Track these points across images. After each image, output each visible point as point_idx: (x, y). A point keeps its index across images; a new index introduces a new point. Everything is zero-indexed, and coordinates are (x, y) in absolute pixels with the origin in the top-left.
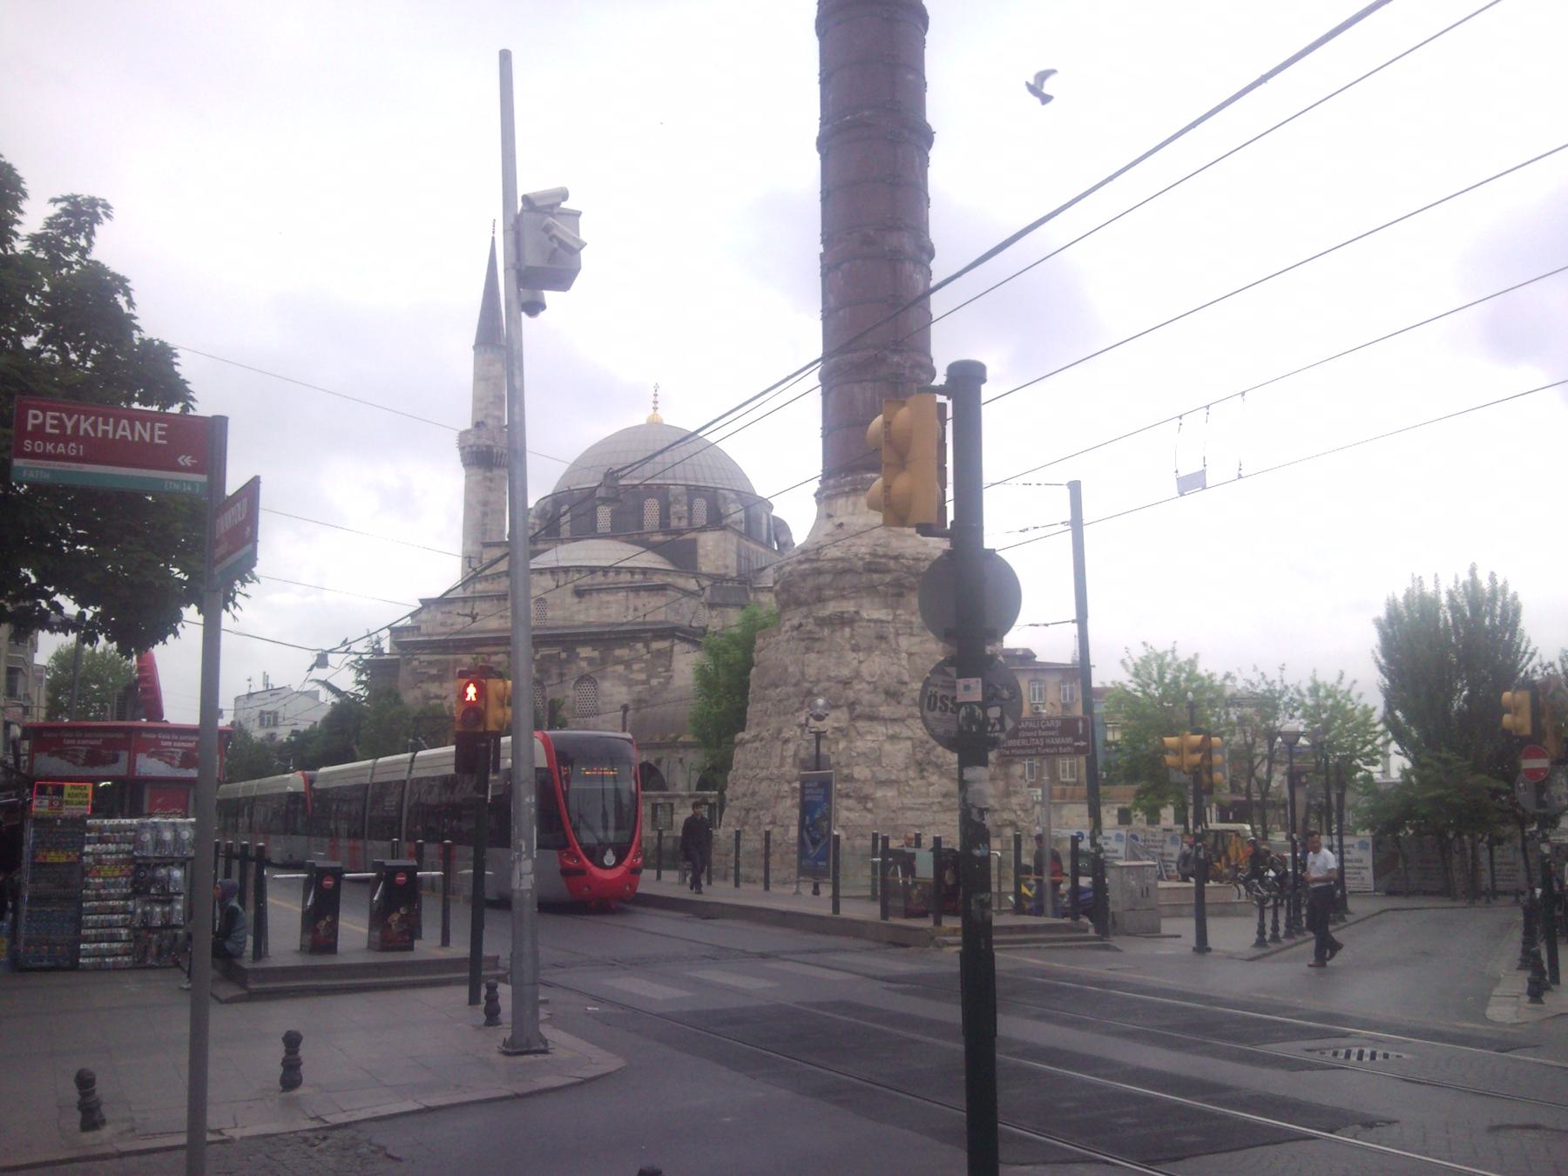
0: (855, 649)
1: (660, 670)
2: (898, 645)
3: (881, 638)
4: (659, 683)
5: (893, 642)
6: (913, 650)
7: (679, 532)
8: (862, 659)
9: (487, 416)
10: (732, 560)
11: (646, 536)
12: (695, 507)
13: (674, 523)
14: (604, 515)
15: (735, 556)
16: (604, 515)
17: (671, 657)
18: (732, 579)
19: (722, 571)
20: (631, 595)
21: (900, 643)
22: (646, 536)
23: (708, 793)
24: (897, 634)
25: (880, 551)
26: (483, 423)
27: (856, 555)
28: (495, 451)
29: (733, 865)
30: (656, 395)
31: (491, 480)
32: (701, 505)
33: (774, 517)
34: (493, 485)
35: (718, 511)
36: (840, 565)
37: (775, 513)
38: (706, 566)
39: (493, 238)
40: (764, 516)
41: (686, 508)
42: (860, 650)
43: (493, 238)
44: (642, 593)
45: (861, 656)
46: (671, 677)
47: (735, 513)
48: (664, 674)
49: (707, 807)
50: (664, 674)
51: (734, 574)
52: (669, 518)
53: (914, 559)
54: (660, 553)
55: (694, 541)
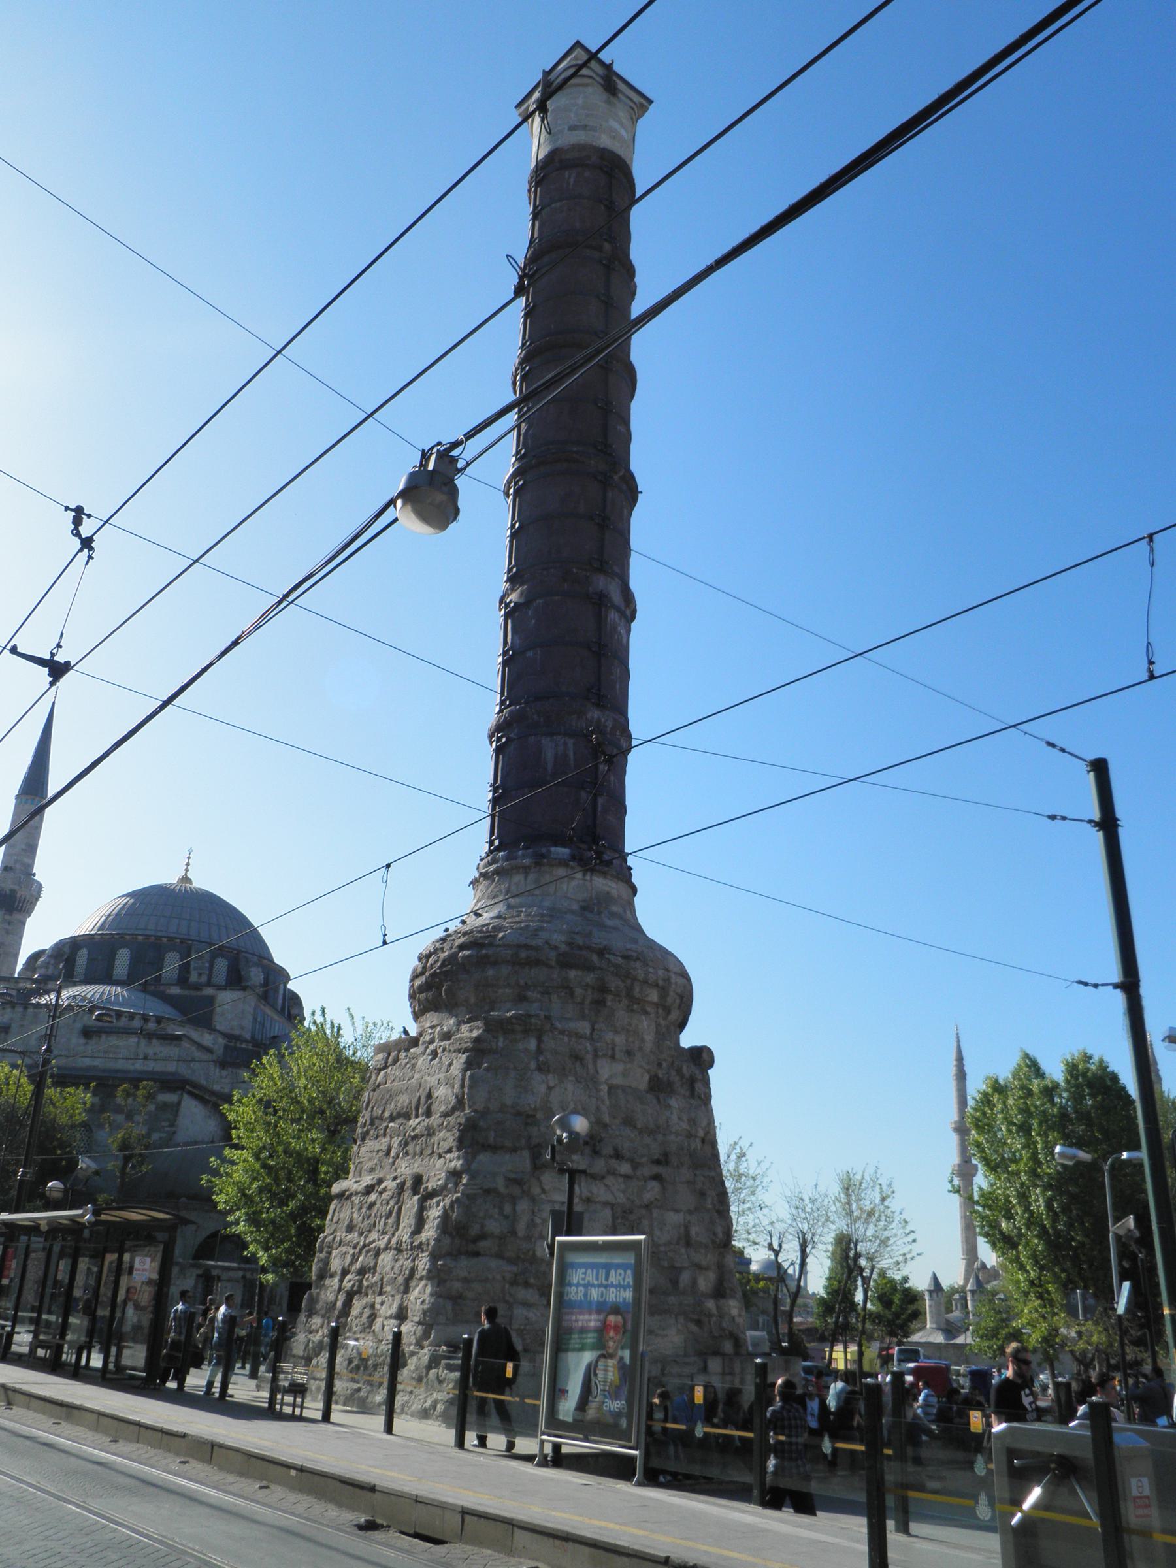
0: (542, 1069)
1: (164, 1124)
2: (597, 1072)
3: (577, 1058)
4: (161, 1138)
5: (590, 1066)
6: (618, 1081)
7: (197, 987)
8: (551, 1084)
9: (16, 861)
10: (247, 1023)
11: (162, 988)
12: (216, 967)
13: (193, 978)
14: (123, 958)
15: (250, 1018)
16: (123, 958)
17: (177, 1111)
18: (246, 1041)
19: (237, 1032)
20: (143, 1042)
21: (601, 1071)
22: (162, 988)
23: (212, 1263)
24: (596, 1056)
25: (580, 941)
26: (11, 868)
27: (547, 943)
28: (18, 895)
29: (324, 1375)
30: (189, 858)
31: (9, 923)
32: (222, 965)
33: (290, 990)
34: (10, 928)
35: (239, 971)
36: (523, 954)
37: (291, 986)
38: (221, 1024)
39: (54, 703)
40: (282, 986)
41: (207, 965)
42: (549, 1071)
43: (54, 703)
44: (155, 1041)
45: (552, 1080)
46: (175, 1133)
47: (256, 976)
48: (166, 1129)
49: (773, 1257)
50: (166, 1129)
51: (248, 1036)
52: (188, 972)
53: (624, 957)
54: (173, 1006)
55: (211, 1000)
